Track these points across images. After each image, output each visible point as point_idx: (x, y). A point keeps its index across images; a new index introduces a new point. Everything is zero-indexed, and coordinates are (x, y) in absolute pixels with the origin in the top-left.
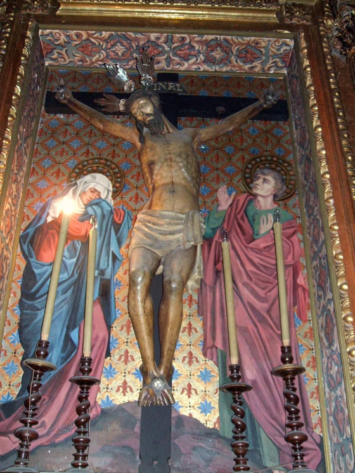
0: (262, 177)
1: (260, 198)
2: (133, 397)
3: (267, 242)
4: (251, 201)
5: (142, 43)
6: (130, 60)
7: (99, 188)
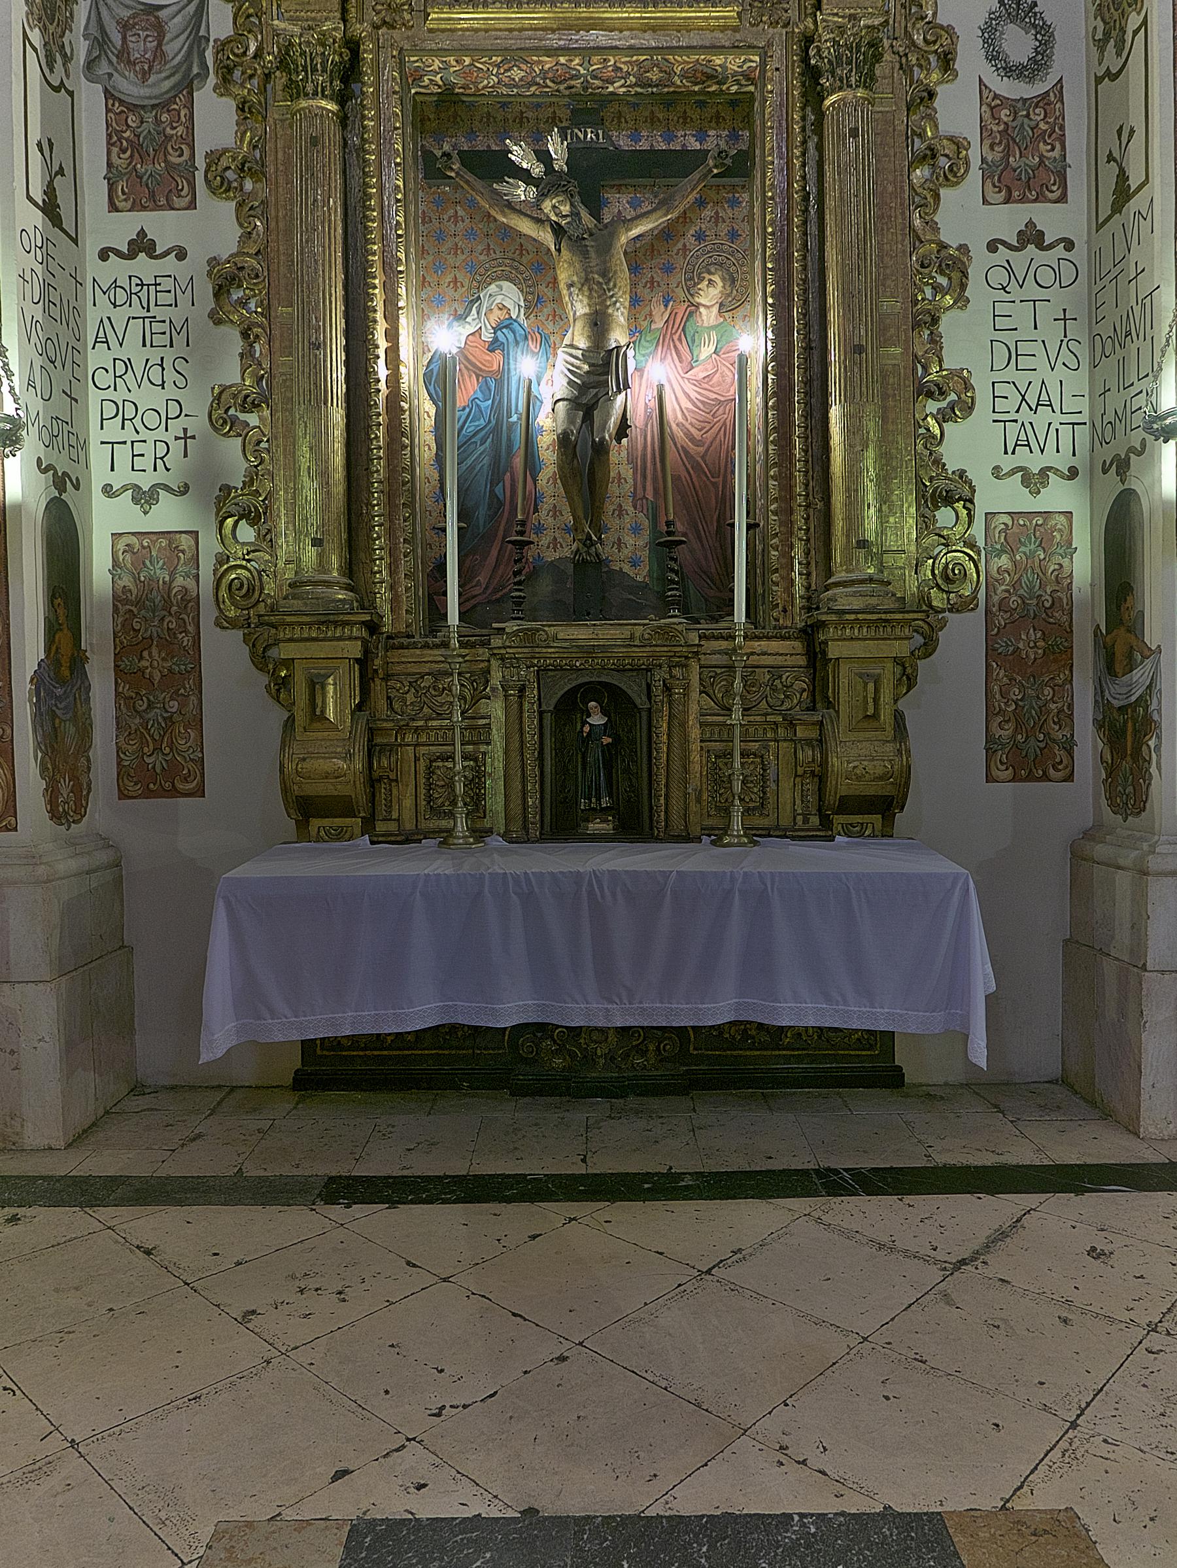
0: (707, 276)
1: (702, 309)
2: (567, 552)
3: (707, 370)
4: (691, 313)
5: (547, 66)
6: (531, 86)
7: (508, 304)
